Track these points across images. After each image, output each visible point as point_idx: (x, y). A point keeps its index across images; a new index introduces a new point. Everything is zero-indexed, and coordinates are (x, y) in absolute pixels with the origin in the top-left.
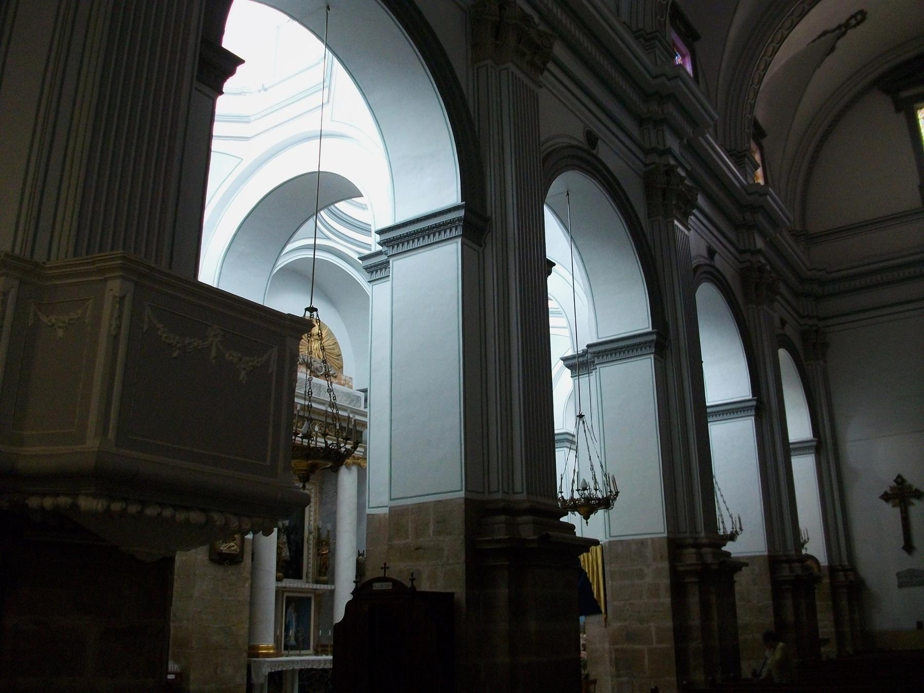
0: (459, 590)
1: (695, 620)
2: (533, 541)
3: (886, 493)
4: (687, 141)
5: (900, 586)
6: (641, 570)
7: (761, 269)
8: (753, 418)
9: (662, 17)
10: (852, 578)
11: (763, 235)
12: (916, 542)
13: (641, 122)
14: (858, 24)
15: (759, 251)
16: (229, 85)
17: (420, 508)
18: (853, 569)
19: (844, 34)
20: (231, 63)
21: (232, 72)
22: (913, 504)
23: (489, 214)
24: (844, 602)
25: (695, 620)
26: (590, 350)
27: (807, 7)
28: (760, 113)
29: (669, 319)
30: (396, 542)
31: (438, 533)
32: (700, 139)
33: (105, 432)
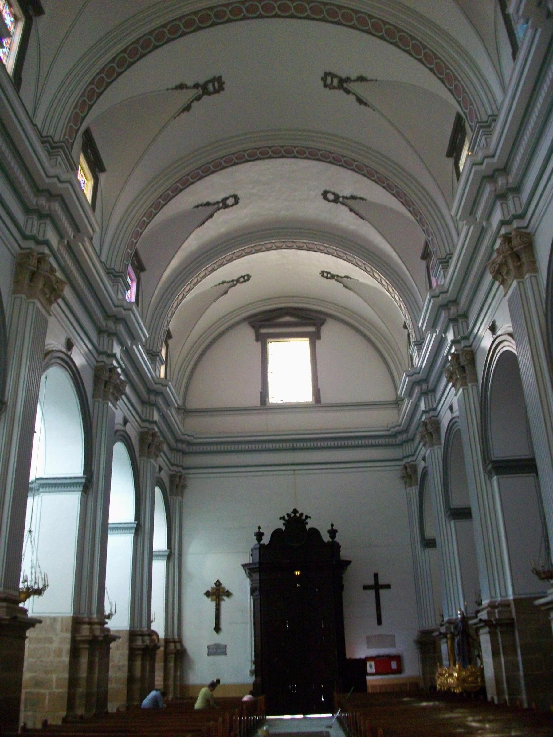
1: (83, 674)
2: (7, 620)
3: (208, 592)
4: (68, 242)
5: (208, 655)
6: (51, 638)
7: (154, 435)
8: (80, 493)
10: (179, 647)
11: (159, 410)
12: (223, 625)
13: (100, 331)
14: (245, 281)
15: (155, 423)
18: (180, 641)
19: (234, 285)
22: (224, 600)
23: (6, 400)
24: (172, 664)
25: (83, 674)
27: (216, 267)
28: (171, 327)
29: (95, 468)
32: (135, 347)
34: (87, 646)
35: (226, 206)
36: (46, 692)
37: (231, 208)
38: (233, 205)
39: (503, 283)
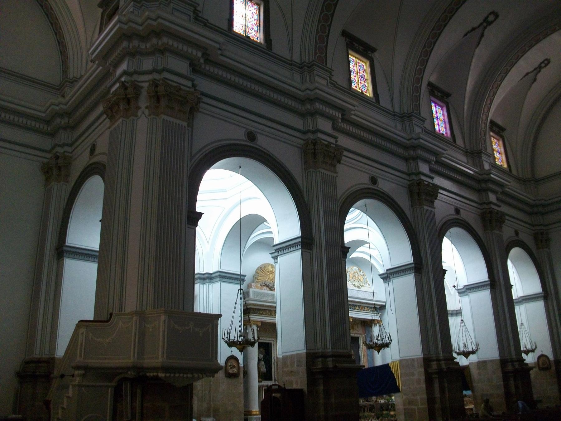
0: (305, 388)
1: (437, 395)
8: (489, 290)
9: (417, 102)
13: (406, 159)
16: (200, 223)
17: (292, 356)
19: (540, 71)
20: (200, 215)
21: (200, 218)
25: (437, 395)
26: (388, 272)
30: (285, 369)
31: (298, 366)
33: (163, 357)
34: (436, 376)
35: (490, 23)
36: (416, 407)
37: (494, 23)
38: (495, 20)
39: (112, 118)
